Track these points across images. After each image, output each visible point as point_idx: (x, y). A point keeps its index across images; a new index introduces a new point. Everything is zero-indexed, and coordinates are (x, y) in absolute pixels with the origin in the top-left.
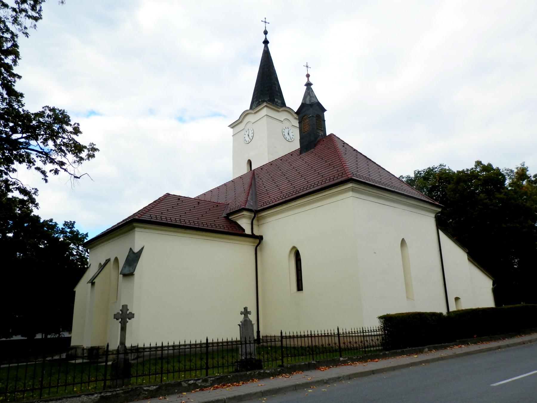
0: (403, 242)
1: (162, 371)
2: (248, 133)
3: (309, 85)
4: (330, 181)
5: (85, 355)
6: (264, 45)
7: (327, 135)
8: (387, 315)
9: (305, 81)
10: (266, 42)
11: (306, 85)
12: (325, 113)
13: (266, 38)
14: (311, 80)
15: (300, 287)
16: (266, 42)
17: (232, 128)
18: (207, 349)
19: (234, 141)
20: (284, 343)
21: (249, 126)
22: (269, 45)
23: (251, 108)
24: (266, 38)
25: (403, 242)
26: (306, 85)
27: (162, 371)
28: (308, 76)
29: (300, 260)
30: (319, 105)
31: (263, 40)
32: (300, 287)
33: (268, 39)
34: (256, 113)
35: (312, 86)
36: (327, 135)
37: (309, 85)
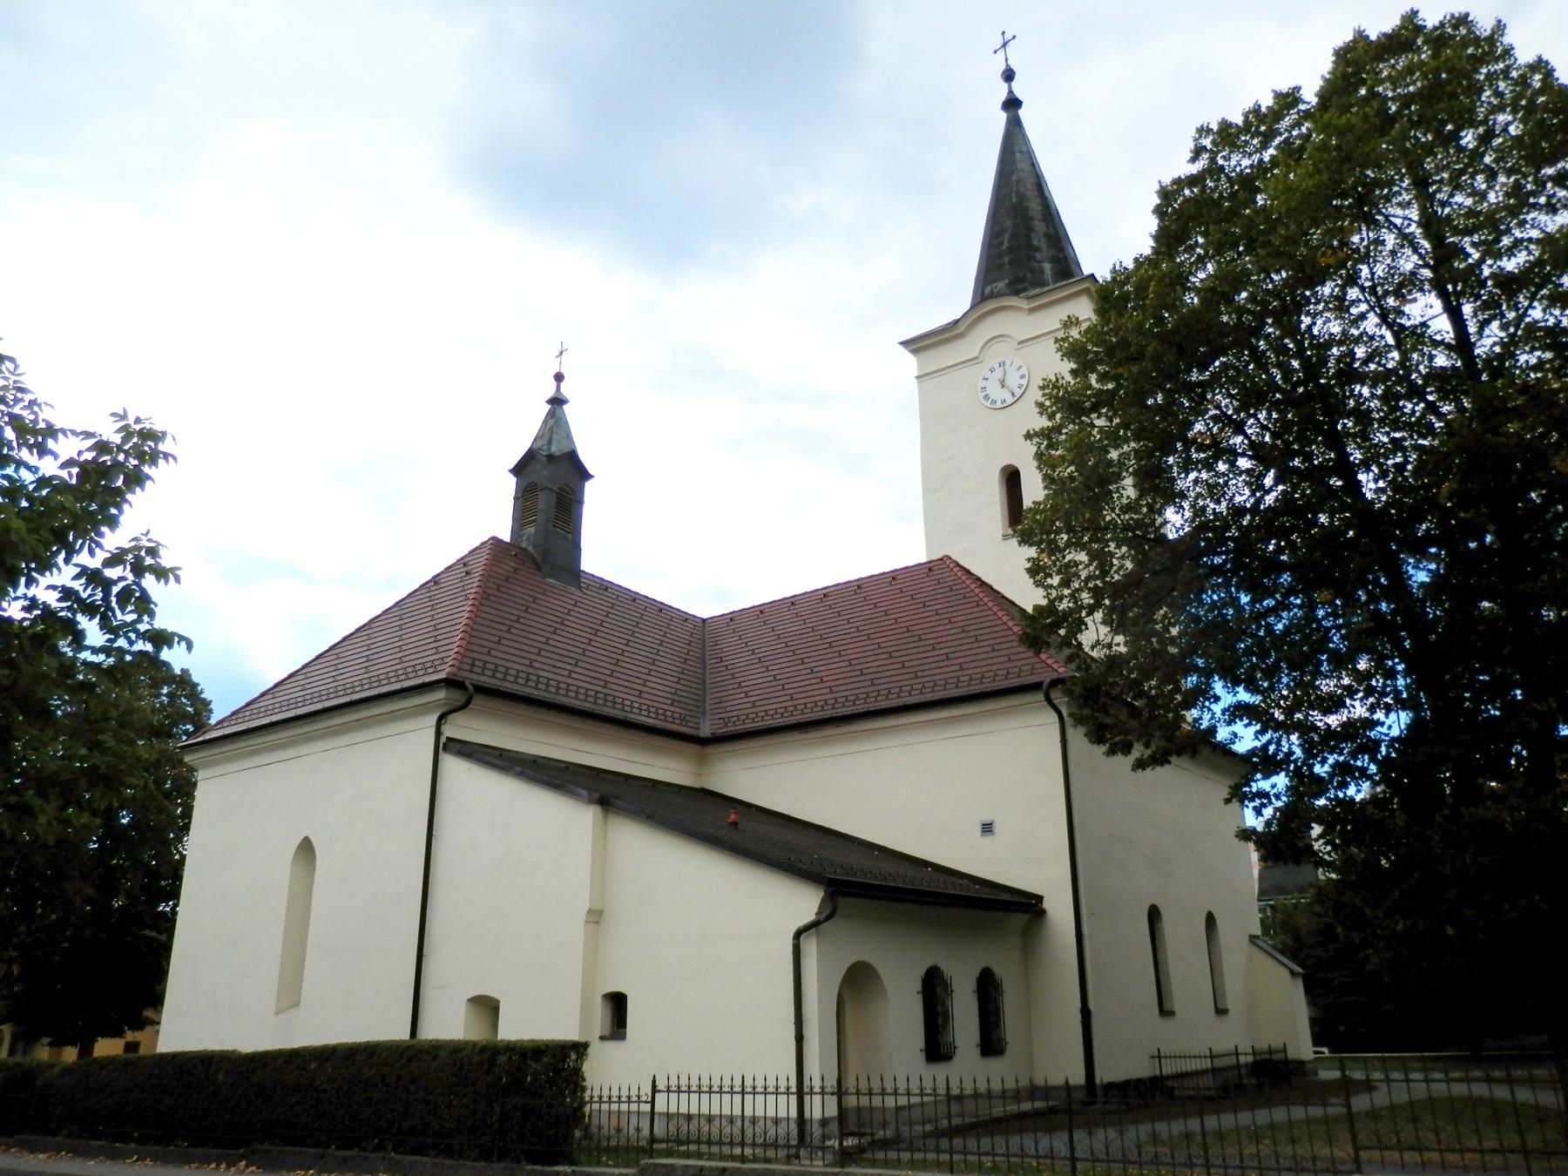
0: (306, 848)
1: (1352, 1126)
2: (999, 373)
3: (557, 402)
4: (483, 674)
8: (234, 1052)
10: (1012, 104)
11: (549, 402)
12: (588, 485)
13: (1011, 92)
14: (565, 389)
16: (1012, 104)
17: (915, 352)
19: (922, 392)
20: (660, 1106)
21: (1001, 351)
24: (1011, 92)
25: (306, 848)
26: (549, 402)
27: (1352, 1126)
28: (559, 378)
29: (945, 905)
30: (572, 458)
31: (1003, 96)
32: (1154, 915)
34: (1032, 310)
35: (565, 407)
37: (557, 402)
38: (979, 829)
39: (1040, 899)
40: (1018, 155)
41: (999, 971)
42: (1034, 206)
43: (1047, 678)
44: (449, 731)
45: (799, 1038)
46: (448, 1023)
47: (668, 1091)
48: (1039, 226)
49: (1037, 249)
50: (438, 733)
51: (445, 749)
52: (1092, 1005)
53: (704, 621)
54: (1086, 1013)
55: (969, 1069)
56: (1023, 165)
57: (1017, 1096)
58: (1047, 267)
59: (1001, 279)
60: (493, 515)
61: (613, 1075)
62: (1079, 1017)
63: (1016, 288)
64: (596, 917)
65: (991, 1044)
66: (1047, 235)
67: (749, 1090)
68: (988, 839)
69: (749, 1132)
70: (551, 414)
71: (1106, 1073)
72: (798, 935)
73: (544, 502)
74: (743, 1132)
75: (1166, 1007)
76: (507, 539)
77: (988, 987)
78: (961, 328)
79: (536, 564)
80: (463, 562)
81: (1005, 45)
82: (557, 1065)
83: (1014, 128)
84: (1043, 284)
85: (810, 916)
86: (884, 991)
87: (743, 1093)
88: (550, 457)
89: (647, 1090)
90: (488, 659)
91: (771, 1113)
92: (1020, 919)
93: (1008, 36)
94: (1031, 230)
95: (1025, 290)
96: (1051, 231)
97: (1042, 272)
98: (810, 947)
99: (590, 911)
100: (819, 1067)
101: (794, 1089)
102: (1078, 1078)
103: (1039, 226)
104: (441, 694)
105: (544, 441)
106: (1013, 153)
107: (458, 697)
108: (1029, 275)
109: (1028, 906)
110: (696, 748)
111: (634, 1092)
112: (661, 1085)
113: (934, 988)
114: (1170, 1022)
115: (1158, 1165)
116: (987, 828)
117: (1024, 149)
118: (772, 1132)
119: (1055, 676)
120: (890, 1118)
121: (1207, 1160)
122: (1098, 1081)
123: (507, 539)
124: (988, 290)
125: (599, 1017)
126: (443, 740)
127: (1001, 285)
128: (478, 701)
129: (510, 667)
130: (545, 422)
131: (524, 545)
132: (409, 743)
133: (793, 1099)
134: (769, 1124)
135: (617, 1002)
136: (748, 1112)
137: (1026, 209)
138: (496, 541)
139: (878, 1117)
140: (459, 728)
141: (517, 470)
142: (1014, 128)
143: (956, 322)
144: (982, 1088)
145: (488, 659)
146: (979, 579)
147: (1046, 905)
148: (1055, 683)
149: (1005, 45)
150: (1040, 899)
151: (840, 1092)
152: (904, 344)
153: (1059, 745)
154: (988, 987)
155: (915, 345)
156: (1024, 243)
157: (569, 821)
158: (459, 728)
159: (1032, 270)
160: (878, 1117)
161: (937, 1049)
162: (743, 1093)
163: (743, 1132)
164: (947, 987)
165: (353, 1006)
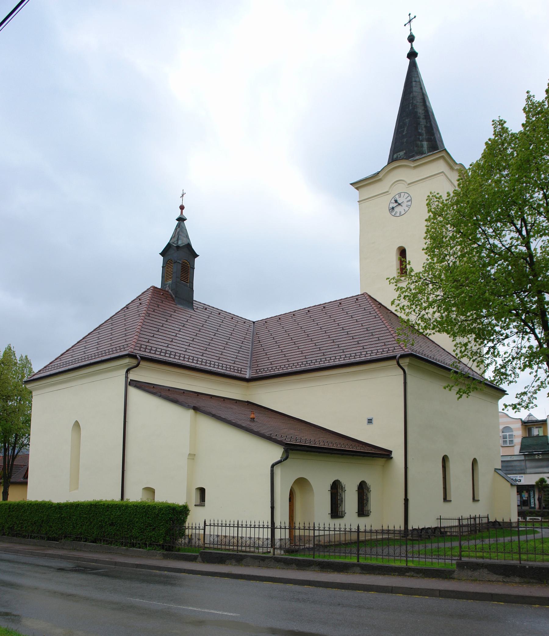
0: (77, 425)
3: (181, 220)
5: (522, 562)
6: (408, 60)
7: (160, 287)
9: (178, 215)
10: (412, 55)
11: (177, 220)
13: (412, 48)
14: (185, 213)
15: (445, 459)
16: (412, 55)
18: (358, 551)
20: (207, 532)
22: (417, 59)
23: (392, 159)
24: (412, 48)
25: (77, 425)
26: (177, 220)
28: (182, 208)
30: (189, 246)
31: (408, 50)
32: (445, 459)
33: (416, 49)
34: (415, 167)
36: (160, 287)
37: (181, 220)
38: (366, 421)
39: (391, 452)
40: (414, 83)
41: (368, 482)
42: (420, 111)
43: (398, 353)
44: (132, 376)
45: (272, 508)
46: (135, 496)
47: (281, 528)
48: (423, 122)
49: (420, 134)
50: (127, 377)
51: (130, 384)
52: (410, 497)
53: (254, 322)
54: (406, 500)
55: (351, 520)
56: (416, 89)
57: (383, 532)
58: (425, 144)
59: (402, 150)
60: (151, 274)
61: (196, 518)
62: (403, 502)
63: (409, 156)
64: (192, 456)
65: (363, 511)
66: (426, 127)
67: (240, 526)
68: (370, 426)
69: (240, 541)
70: (178, 226)
71: (413, 524)
72: (273, 466)
73: (176, 268)
74: (238, 541)
75: (476, 499)
76: (159, 286)
77: (363, 490)
78: (381, 175)
79: (172, 298)
80: (139, 298)
81: (410, 22)
82: (177, 514)
83: (413, 68)
84: (422, 153)
85: (278, 458)
86: (313, 490)
87: (238, 527)
88: (178, 247)
89: (202, 526)
90: (148, 344)
91: (224, 534)
92: (381, 461)
93: (412, 16)
94: (418, 124)
95: (413, 156)
96: (428, 125)
97: (422, 146)
98: (278, 471)
99: (190, 454)
100: (282, 518)
101: (270, 526)
102: (403, 528)
103: (423, 122)
104: (127, 361)
105: (175, 239)
106: (411, 82)
107: (134, 362)
108: (416, 149)
109: (386, 455)
110: (245, 384)
111: (197, 526)
112: (208, 523)
113: (336, 489)
114: (447, 505)
115: (351, 553)
116: (370, 421)
117: (417, 80)
118: (248, 542)
119: (402, 352)
120: (312, 539)
121: (407, 554)
122: (410, 528)
123: (159, 286)
124: (395, 156)
125: (194, 498)
126: (129, 380)
127: (402, 153)
128: (143, 363)
129: (159, 347)
130: (176, 229)
131: (167, 289)
132: (113, 382)
133: (270, 530)
134: (215, 537)
135: (202, 491)
136: (240, 535)
137: (416, 112)
138: (155, 288)
139: (306, 538)
140: (134, 376)
141: (163, 254)
142: (413, 68)
143: (378, 173)
144: (368, 529)
145: (148, 344)
146: (380, 304)
147: (393, 455)
148: (402, 356)
149: (410, 22)
150: (391, 452)
151: (292, 528)
152: (351, 184)
153: (403, 384)
154: (363, 490)
155: (358, 185)
156: (415, 131)
157: (176, 420)
158: (134, 376)
159: (417, 146)
160: (306, 538)
161: (336, 511)
162: (238, 527)
163: (238, 541)
164: (343, 489)
165: (98, 487)
